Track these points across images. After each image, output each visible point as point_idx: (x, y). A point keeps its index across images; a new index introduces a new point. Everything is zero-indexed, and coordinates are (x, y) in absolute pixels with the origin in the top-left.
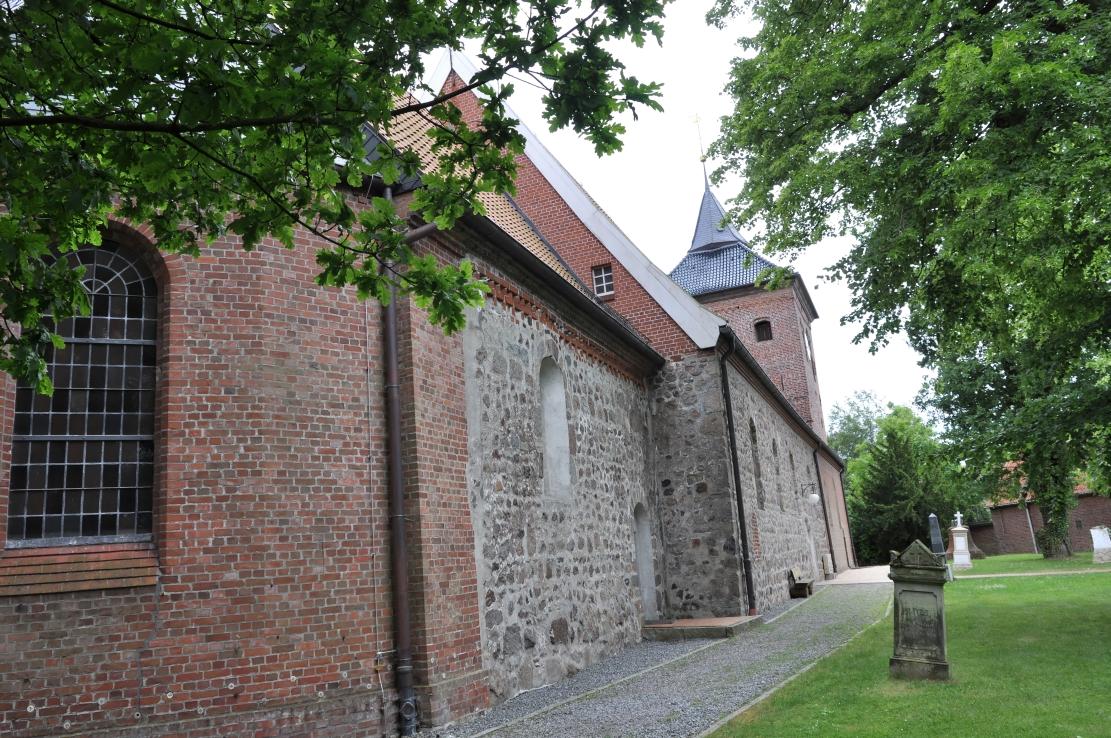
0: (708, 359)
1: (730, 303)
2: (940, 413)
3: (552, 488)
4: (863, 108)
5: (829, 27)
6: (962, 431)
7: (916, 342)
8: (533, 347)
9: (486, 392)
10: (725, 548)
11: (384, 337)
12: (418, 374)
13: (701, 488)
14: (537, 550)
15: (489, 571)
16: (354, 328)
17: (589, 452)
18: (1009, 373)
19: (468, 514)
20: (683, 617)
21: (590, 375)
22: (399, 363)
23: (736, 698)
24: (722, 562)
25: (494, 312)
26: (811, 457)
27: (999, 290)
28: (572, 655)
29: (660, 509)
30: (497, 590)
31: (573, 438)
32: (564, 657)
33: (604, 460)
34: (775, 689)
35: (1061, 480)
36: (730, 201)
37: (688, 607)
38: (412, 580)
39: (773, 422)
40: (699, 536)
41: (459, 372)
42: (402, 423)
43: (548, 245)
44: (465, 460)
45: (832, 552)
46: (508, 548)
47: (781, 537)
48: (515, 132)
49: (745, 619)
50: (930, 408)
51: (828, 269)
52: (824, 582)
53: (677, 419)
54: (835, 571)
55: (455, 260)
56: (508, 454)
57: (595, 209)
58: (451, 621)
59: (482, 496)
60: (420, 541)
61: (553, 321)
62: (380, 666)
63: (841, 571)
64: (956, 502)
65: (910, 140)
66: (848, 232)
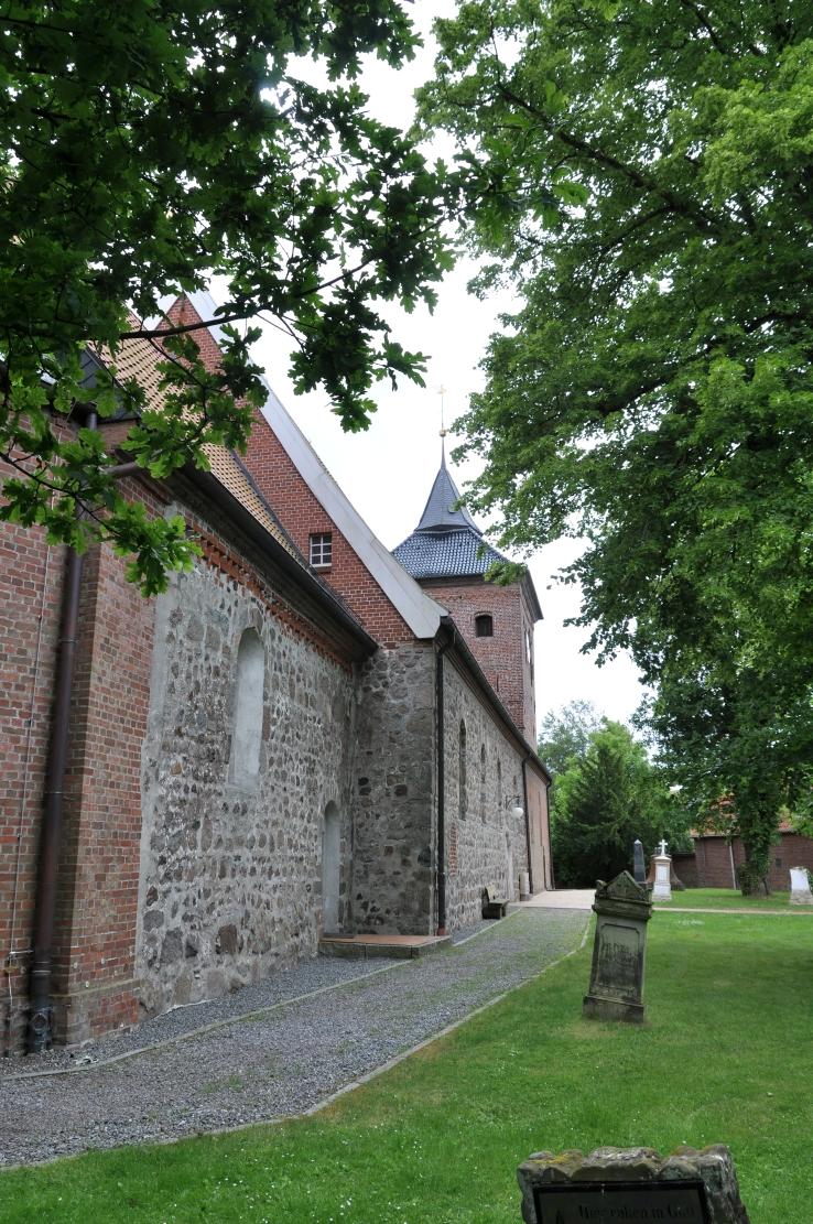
0: (425, 650)
1: (452, 592)
2: (654, 734)
3: (237, 776)
4: (618, 408)
5: (593, 318)
6: (675, 755)
7: (639, 657)
8: (235, 614)
9: (176, 660)
10: (420, 859)
11: (66, 584)
12: (100, 630)
13: (401, 791)
14: (213, 845)
15: (154, 866)
16: (31, 568)
17: (283, 740)
18: (728, 700)
19: (138, 797)
20: (365, 932)
21: (294, 653)
22: (81, 615)
23: (419, 1030)
24: (414, 874)
25: (197, 570)
26: (519, 766)
27: (730, 615)
28: (238, 968)
29: (353, 810)
30: (161, 888)
31: (267, 722)
32: (228, 970)
33: (299, 749)
34: (461, 1022)
35: (769, 817)
36: (468, 483)
37: (373, 920)
38: (62, 869)
39: (485, 726)
40: (393, 844)
41: (149, 633)
42: (74, 685)
43: (265, 503)
44: (141, 734)
45: (530, 871)
46: (179, 839)
47: (480, 851)
48: (257, 380)
49: (432, 939)
50: (646, 728)
51: (563, 570)
52: (518, 904)
53: (383, 711)
54: (531, 892)
55: (160, 507)
56: (192, 732)
57: (321, 471)
58: (103, 920)
59: (157, 777)
60: (78, 824)
61: (262, 589)
62: (12, 968)
63: (537, 893)
64: (661, 829)
65: (662, 447)
66: (585, 533)
